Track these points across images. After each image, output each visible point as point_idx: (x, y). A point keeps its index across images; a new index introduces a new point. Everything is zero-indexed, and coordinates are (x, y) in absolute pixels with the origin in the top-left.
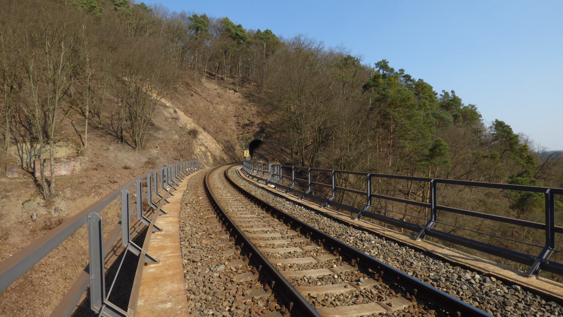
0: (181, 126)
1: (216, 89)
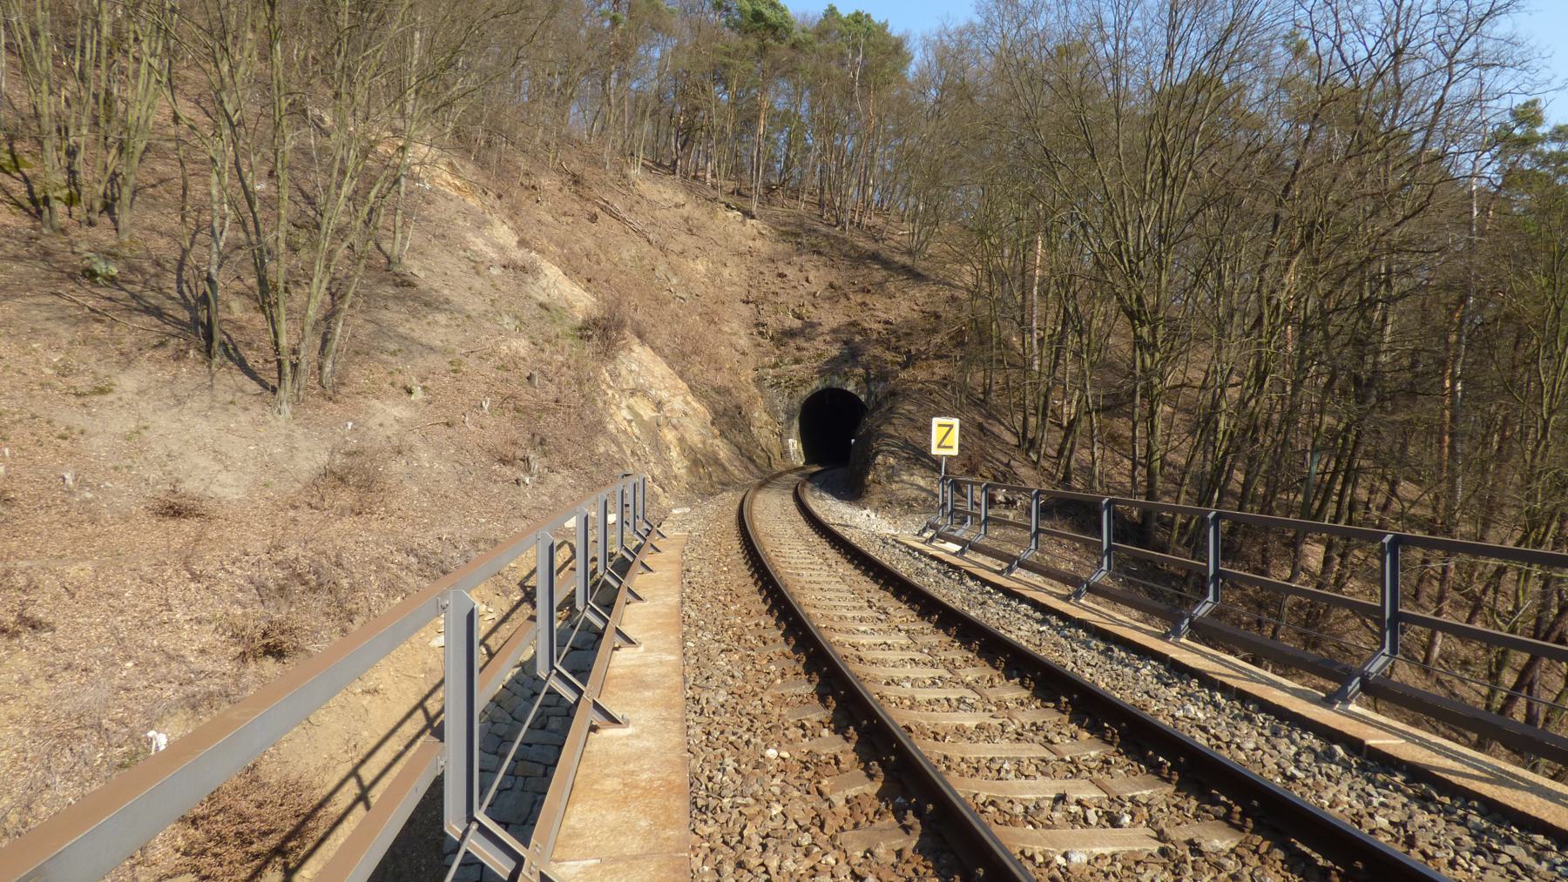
0: (543, 298)
1: (677, 206)
